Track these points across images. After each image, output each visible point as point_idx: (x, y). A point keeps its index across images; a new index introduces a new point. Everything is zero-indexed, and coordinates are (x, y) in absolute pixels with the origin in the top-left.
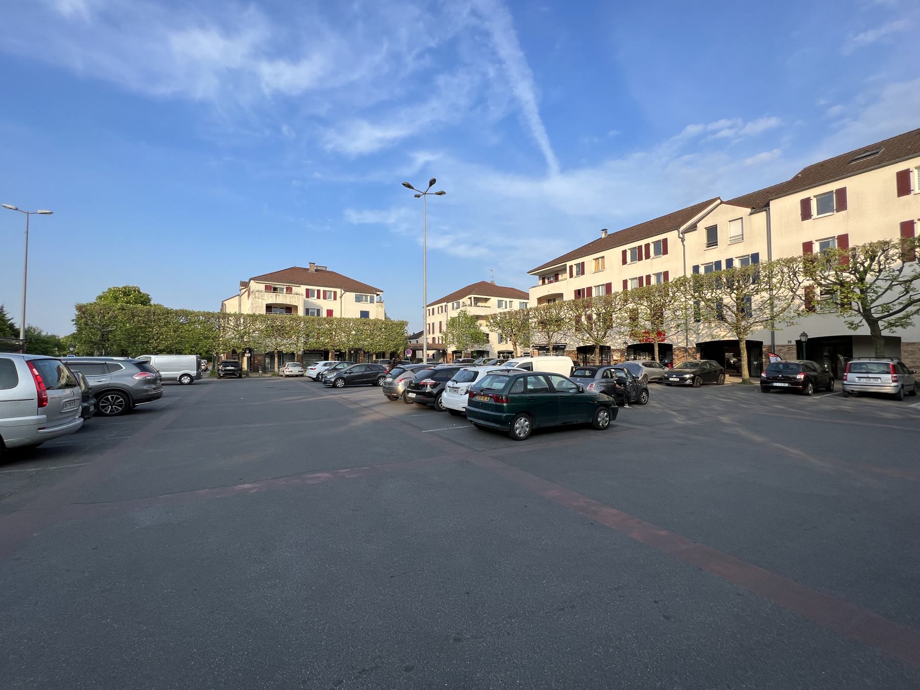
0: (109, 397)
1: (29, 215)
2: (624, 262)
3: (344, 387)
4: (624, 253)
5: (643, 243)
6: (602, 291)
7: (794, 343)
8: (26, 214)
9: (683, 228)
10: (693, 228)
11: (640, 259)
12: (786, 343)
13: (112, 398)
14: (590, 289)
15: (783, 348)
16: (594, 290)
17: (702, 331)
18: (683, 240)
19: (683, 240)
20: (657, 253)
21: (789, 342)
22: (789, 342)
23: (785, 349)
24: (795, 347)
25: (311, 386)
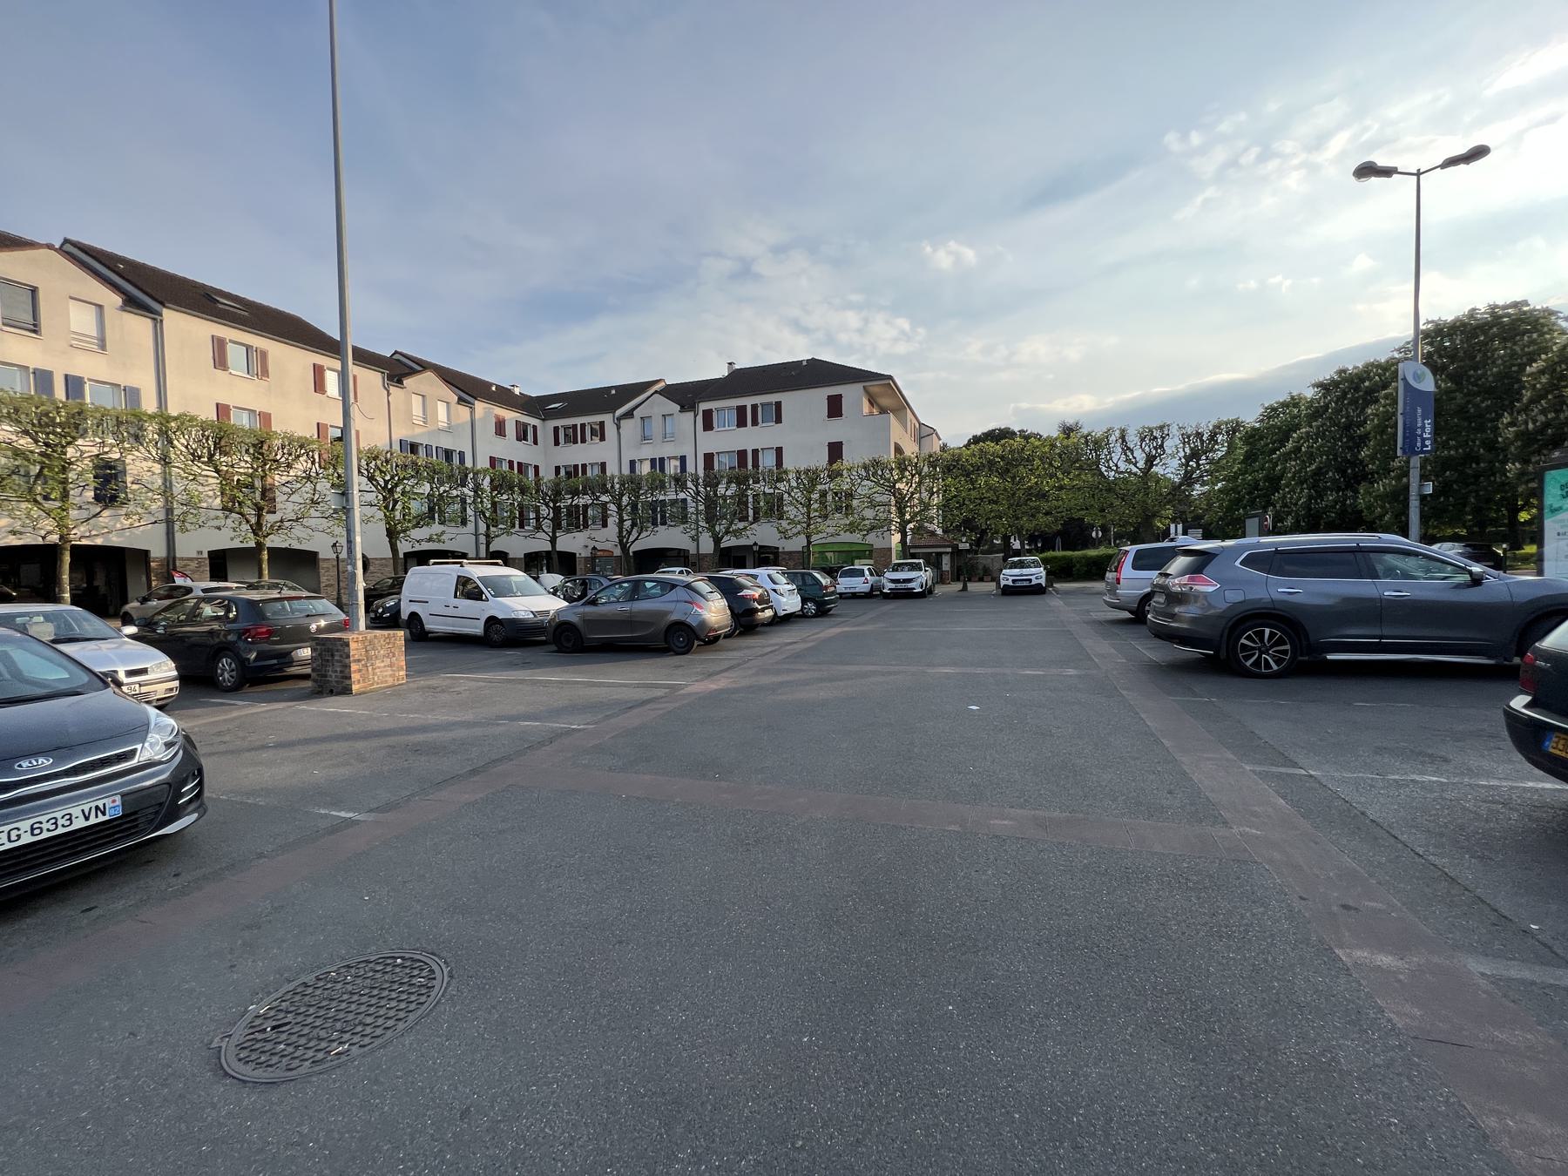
0: (1267, 631)
1: (1415, 177)
2: (557, 443)
3: (815, 616)
4: (556, 429)
5: (578, 421)
6: (597, 470)
7: (205, 555)
8: (1415, 177)
9: (619, 412)
10: (629, 414)
11: (575, 442)
12: (195, 555)
13: (1272, 635)
14: (584, 466)
15: (189, 563)
16: (589, 469)
17: (628, 539)
18: (618, 428)
19: (618, 428)
20: (568, 439)
21: (198, 552)
22: (198, 552)
23: (194, 565)
24: (207, 562)
25: (1223, 631)
